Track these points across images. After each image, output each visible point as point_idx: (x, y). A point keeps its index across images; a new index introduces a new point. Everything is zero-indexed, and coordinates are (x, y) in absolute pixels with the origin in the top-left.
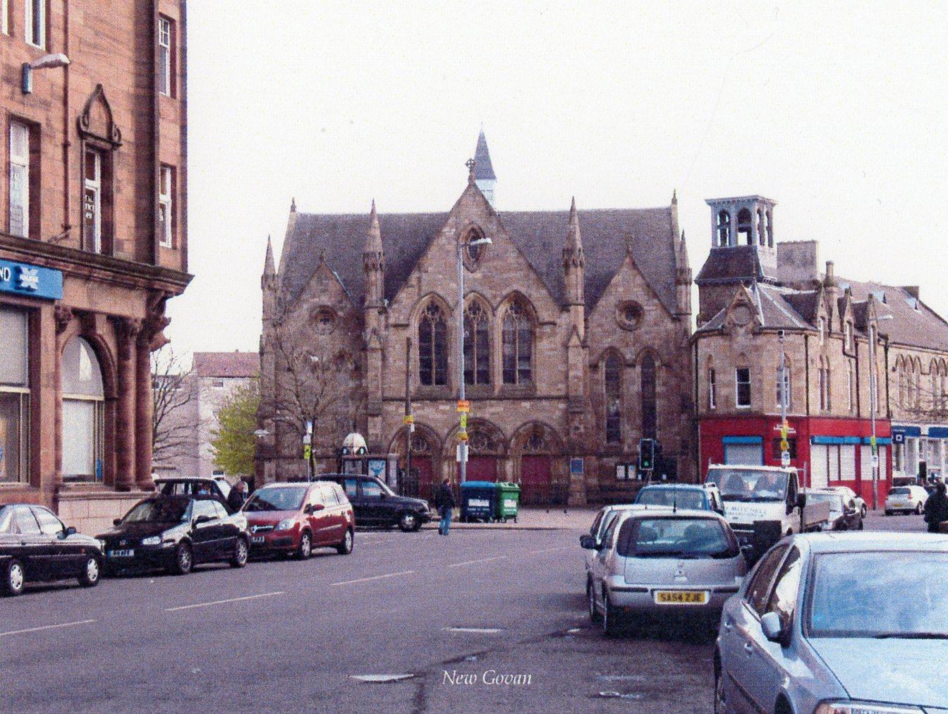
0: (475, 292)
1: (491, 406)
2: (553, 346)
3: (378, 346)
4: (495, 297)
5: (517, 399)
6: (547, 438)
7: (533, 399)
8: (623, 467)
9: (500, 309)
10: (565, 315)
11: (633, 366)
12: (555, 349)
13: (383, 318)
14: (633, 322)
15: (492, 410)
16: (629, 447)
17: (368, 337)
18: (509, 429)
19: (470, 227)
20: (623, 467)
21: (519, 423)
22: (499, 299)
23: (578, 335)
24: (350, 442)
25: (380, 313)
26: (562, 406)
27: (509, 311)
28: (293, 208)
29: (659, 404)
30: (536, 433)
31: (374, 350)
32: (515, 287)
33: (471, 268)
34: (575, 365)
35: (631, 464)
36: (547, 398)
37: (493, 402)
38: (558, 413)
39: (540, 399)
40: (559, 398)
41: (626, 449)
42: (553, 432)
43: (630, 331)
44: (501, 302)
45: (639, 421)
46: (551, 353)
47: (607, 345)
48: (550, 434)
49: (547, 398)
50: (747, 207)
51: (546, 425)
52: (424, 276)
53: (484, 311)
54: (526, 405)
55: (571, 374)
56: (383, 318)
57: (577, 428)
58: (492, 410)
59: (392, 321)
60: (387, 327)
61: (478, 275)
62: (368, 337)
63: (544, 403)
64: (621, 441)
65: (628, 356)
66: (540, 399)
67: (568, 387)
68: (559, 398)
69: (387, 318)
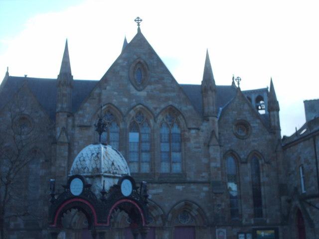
0: (142, 105)
1: (153, 188)
2: (198, 145)
3: (66, 140)
4: (156, 109)
5: (173, 183)
6: (194, 213)
7: (185, 183)
8: (243, 235)
9: (159, 118)
10: (205, 124)
11: (246, 163)
12: (199, 148)
13: (70, 120)
14: (243, 134)
15: (154, 191)
16: (246, 221)
17: (58, 134)
18: (167, 206)
19: (138, 61)
20: (243, 235)
21: (174, 202)
22: (158, 111)
23: (216, 136)
24: (89, 164)
25: (68, 116)
26: (205, 189)
27: (165, 119)
28: (7, 73)
29: (264, 190)
30: (186, 208)
31: (62, 143)
32: (170, 103)
33: (138, 88)
34: (215, 159)
35: (249, 233)
36: (194, 183)
37: (155, 185)
38: (203, 194)
39: (190, 182)
40: (203, 183)
41: (244, 222)
42: (200, 209)
43: (243, 139)
44: (160, 113)
45: (251, 202)
46: (196, 150)
47: (228, 149)
48: (197, 210)
49: (194, 183)
50: (261, 94)
51: (194, 203)
52: (104, 92)
53: (147, 119)
54: (179, 187)
55: (213, 164)
56: (70, 120)
57: (219, 205)
58: (154, 191)
59: (77, 123)
60: (73, 126)
61: (143, 94)
62: (58, 134)
63: (193, 186)
64: (241, 216)
65: (242, 157)
66: (190, 182)
67: (210, 175)
68: (203, 183)
69: (74, 120)
